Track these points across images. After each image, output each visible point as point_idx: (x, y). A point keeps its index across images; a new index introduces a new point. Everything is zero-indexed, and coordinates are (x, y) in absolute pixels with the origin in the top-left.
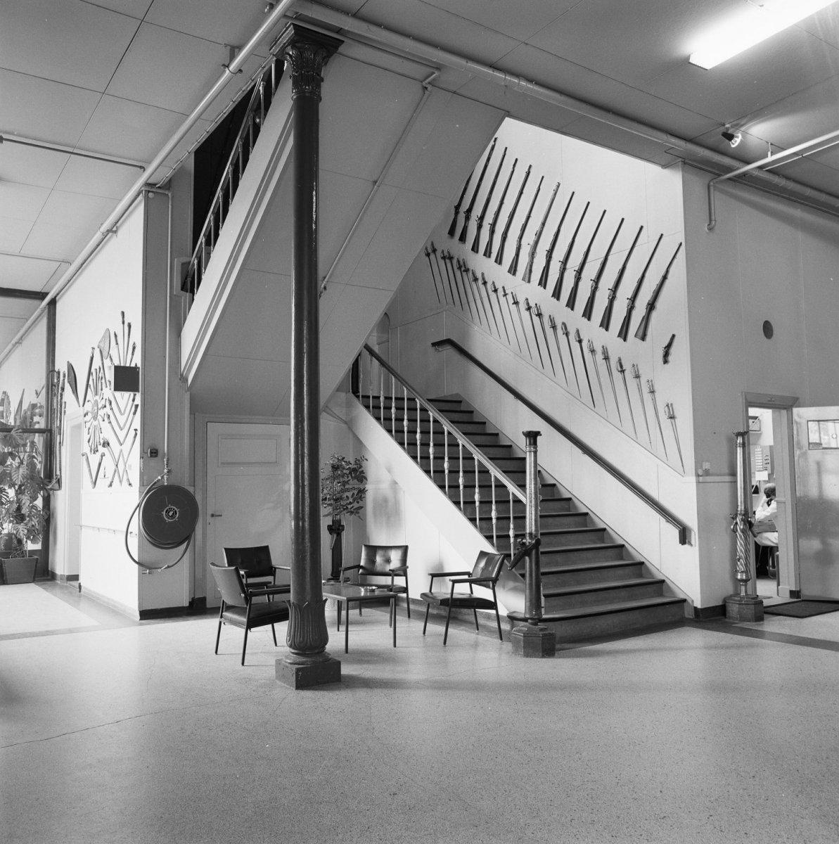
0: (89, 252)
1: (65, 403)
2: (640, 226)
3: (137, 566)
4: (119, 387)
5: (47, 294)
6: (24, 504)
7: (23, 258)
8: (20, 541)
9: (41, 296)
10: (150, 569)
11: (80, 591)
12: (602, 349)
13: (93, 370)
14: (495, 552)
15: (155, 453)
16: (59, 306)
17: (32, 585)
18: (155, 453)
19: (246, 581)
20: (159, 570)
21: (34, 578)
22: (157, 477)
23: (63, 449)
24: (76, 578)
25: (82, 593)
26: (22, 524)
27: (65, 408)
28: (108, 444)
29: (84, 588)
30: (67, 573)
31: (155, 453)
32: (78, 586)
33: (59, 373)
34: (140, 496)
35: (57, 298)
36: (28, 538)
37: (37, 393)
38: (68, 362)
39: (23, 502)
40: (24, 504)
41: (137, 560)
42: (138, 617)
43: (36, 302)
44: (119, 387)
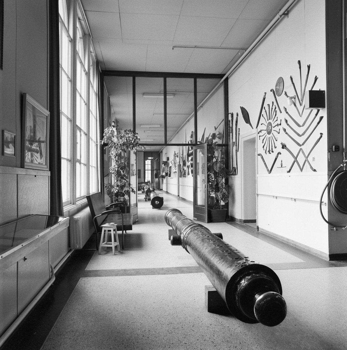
0: (263, 35)
1: (239, 129)
2: (297, 62)
3: (327, 225)
4: (312, 105)
5: (224, 75)
6: (220, 182)
7: (232, 50)
8: (218, 201)
9: (220, 76)
10: (336, 226)
11: (258, 231)
12: (281, 145)
13: (265, 105)
14: (302, 261)
15: (338, 148)
16: (230, 81)
17: (225, 223)
18: (337, 148)
19: (123, 232)
20: (344, 229)
21: (225, 220)
22: (340, 165)
23: (238, 153)
24: (254, 221)
25: (259, 231)
26: (219, 192)
27: (239, 131)
28: (286, 146)
29: (260, 228)
30: (243, 219)
31: (338, 148)
32: (256, 227)
33: (232, 115)
34: (329, 176)
35: (229, 77)
36: (222, 199)
37: (215, 128)
38: (240, 107)
39: (219, 181)
40: (220, 182)
41: (327, 220)
42: (328, 259)
43: (218, 80)
44: (312, 105)
